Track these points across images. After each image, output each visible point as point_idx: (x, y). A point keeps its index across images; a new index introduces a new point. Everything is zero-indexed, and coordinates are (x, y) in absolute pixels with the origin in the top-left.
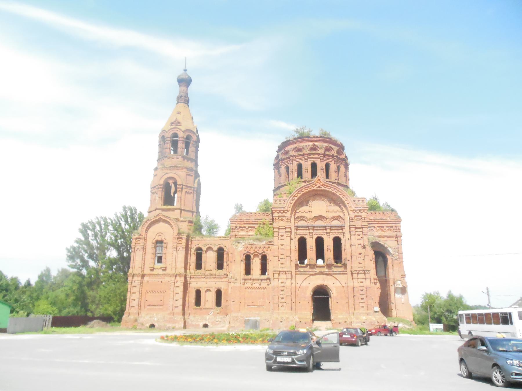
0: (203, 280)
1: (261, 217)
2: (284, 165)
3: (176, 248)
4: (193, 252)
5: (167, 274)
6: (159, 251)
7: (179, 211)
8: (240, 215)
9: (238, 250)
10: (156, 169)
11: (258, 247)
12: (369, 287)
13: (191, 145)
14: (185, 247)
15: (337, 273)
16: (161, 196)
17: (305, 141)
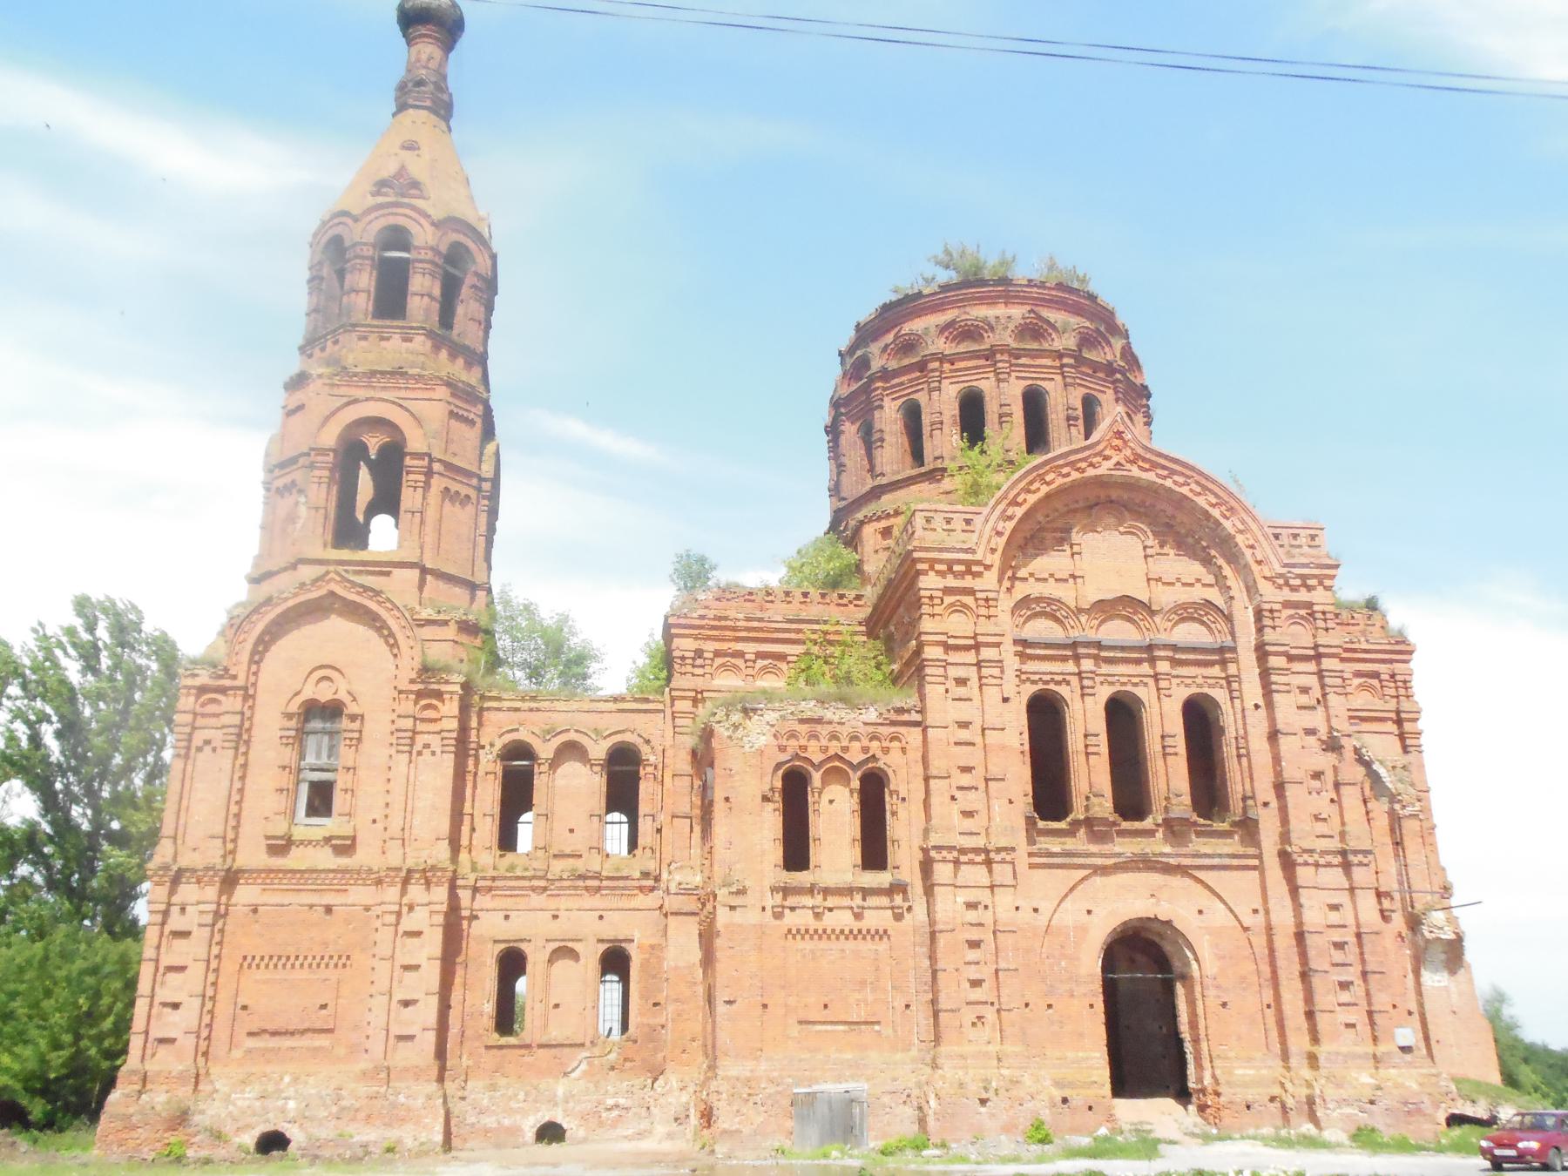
0: (537, 900)
1: (814, 611)
3: (408, 742)
4: (488, 764)
5: (358, 872)
6: (318, 756)
7: (415, 574)
8: (718, 599)
9: (748, 746)
10: (299, 381)
11: (845, 731)
12: (1375, 929)
13: (465, 291)
14: (454, 735)
15: (1216, 861)
16: (322, 503)
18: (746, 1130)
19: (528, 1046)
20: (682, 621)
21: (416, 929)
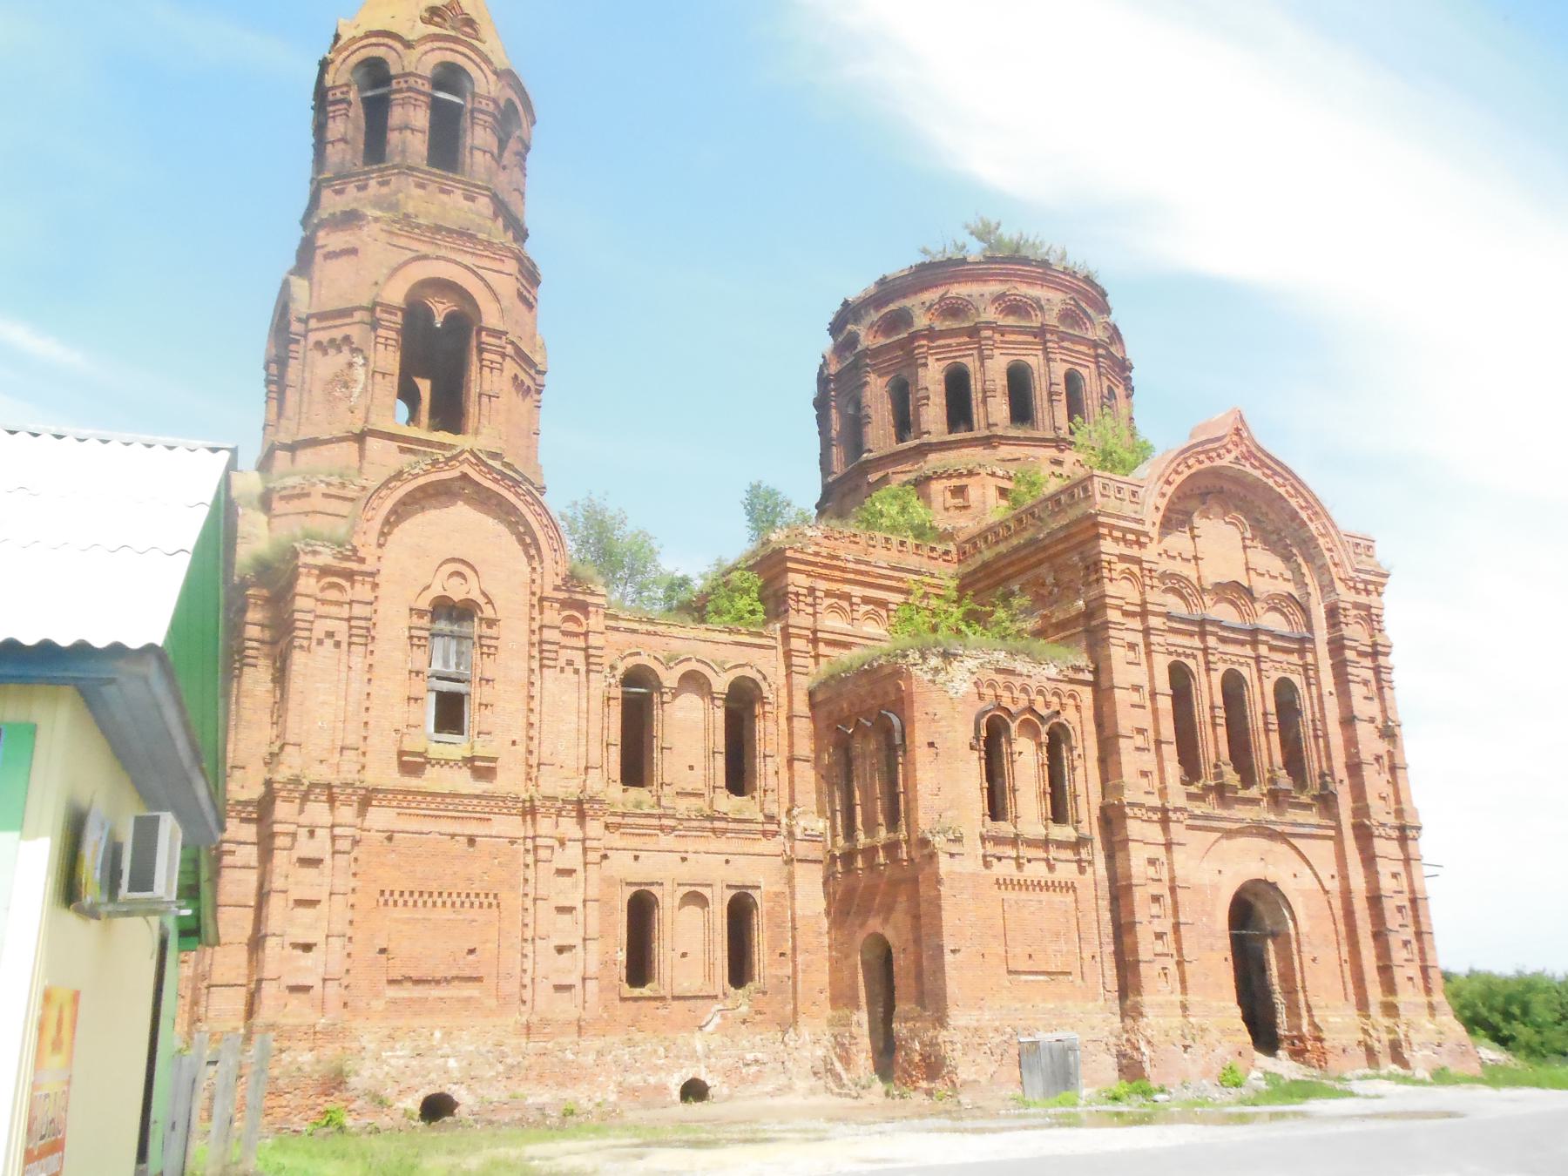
0: (667, 841)
1: (912, 561)
2: (938, 360)
6: (446, 663)
17: (1027, 277)
18: (984, 1080)
19: (663, 998)
20: (799, 556)
21: (568, 867)
